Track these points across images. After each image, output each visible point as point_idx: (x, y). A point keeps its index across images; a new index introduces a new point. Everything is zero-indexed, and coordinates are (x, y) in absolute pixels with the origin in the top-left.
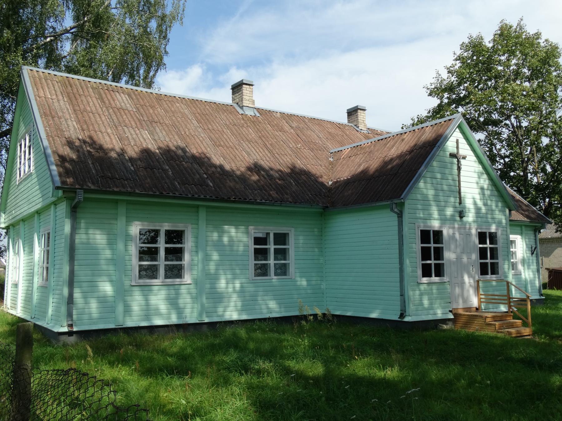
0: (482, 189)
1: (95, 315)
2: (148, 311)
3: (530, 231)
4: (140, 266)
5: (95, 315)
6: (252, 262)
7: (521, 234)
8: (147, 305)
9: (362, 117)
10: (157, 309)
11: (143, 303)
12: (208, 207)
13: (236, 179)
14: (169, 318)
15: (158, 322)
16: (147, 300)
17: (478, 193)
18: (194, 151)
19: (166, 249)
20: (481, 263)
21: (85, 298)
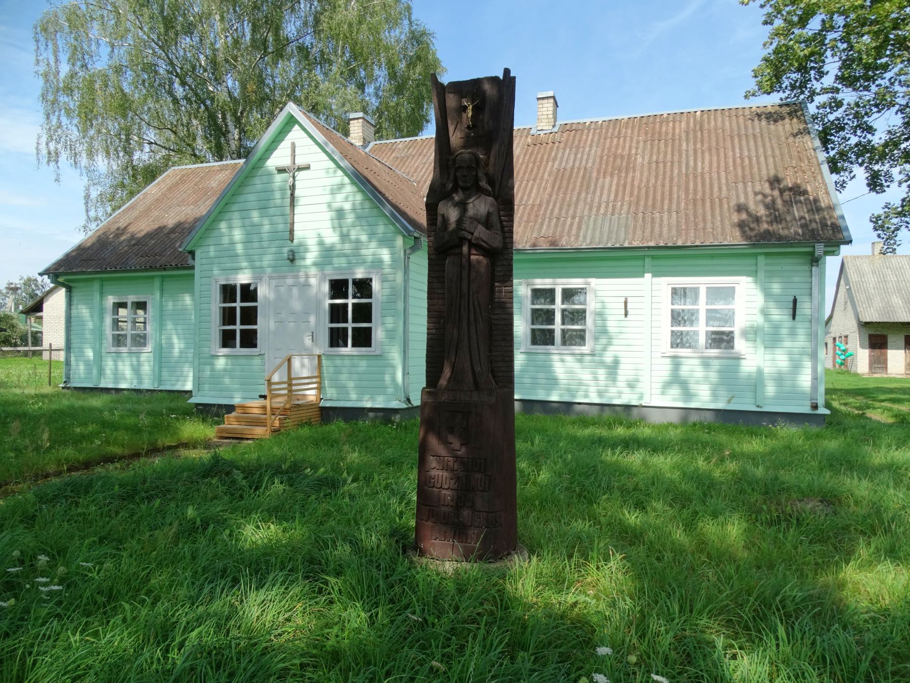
0: (340, 214)
1: (82, 376)
2: (117, 376)
3: (803, 264)
4: (672, 332)
5: (82, 376)
6: (326, 325)
7: (753, 273)
8: (116, 369)
9: (546, 109)
10: (124, 374)
11: (113, 367)
12: (766, 254)
13: (439, 219)
14: (132, 384)
15: (123, 386)
16: (116, 365)
17: (329, 218)
18: (355, 189)
19: (708, 311)
20: (370, 321)
21: (77, 361)
